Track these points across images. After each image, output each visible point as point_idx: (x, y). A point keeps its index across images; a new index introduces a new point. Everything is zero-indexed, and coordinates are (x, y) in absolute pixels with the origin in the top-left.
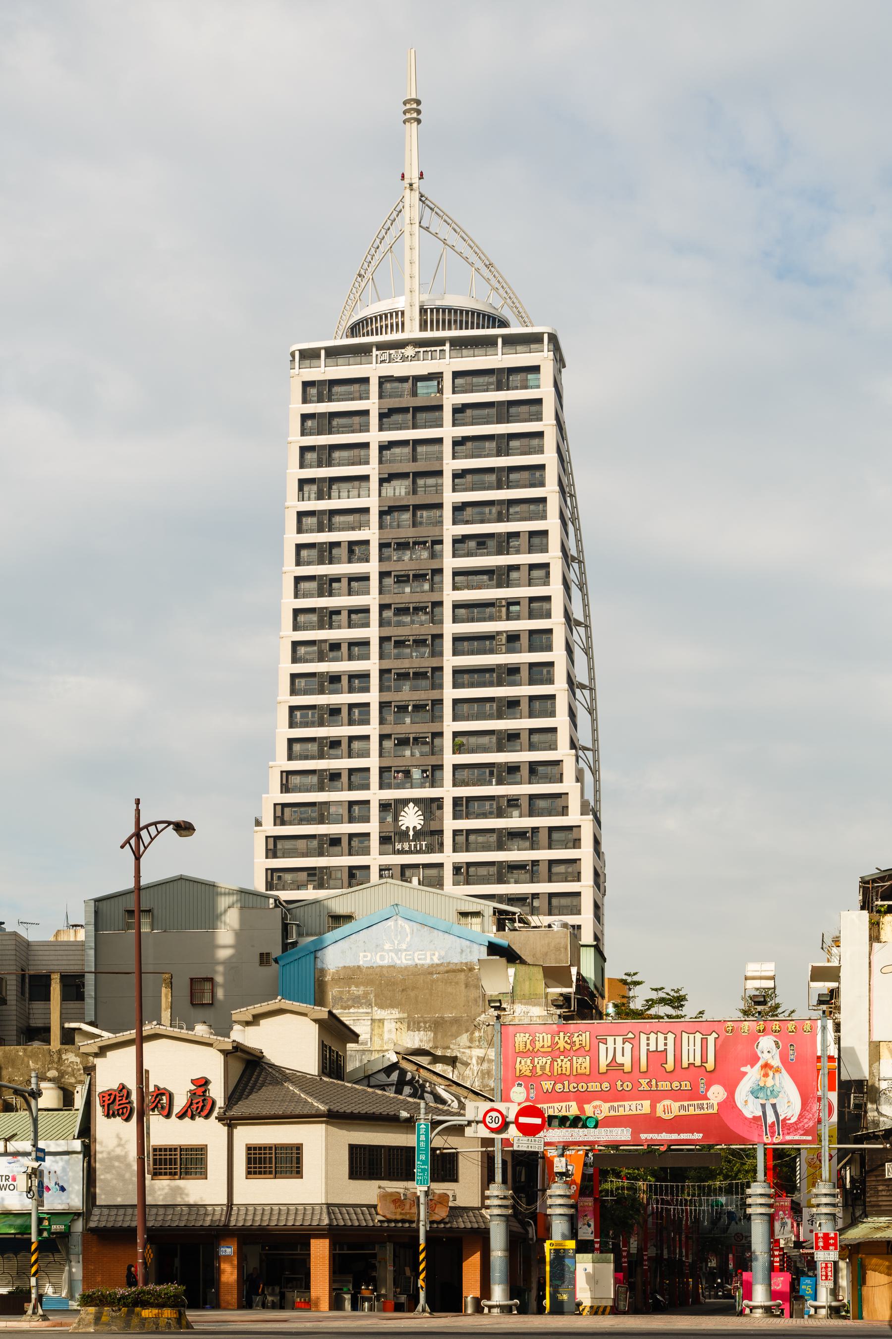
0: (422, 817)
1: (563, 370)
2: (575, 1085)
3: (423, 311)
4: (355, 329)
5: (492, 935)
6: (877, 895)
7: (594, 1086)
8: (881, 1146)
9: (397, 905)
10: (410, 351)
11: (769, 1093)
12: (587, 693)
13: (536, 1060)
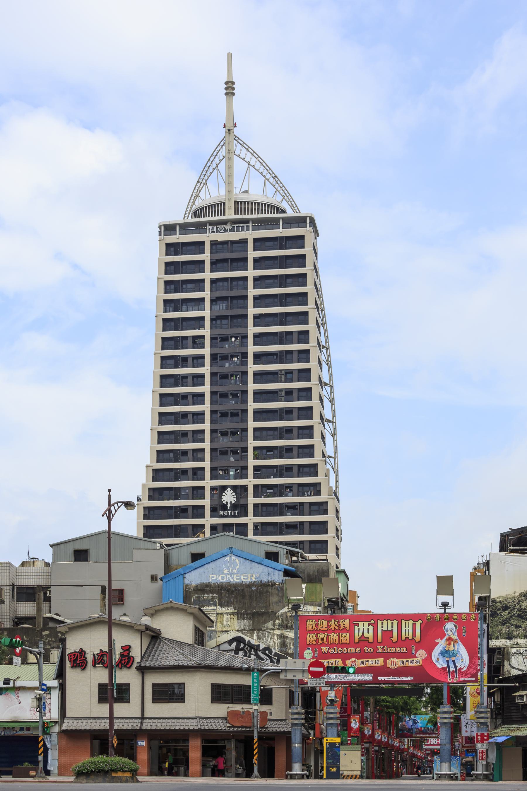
1: (317, 238)
2: (341, 649)
3: (236, 203)
4: (196, 214)
6: (510, 543)
7: (352, 650)
8: (513, 684)
9: (231, 548)
10: (229, 227)
11: (451, 654)
12: (331, 424)
13: (318, 635)
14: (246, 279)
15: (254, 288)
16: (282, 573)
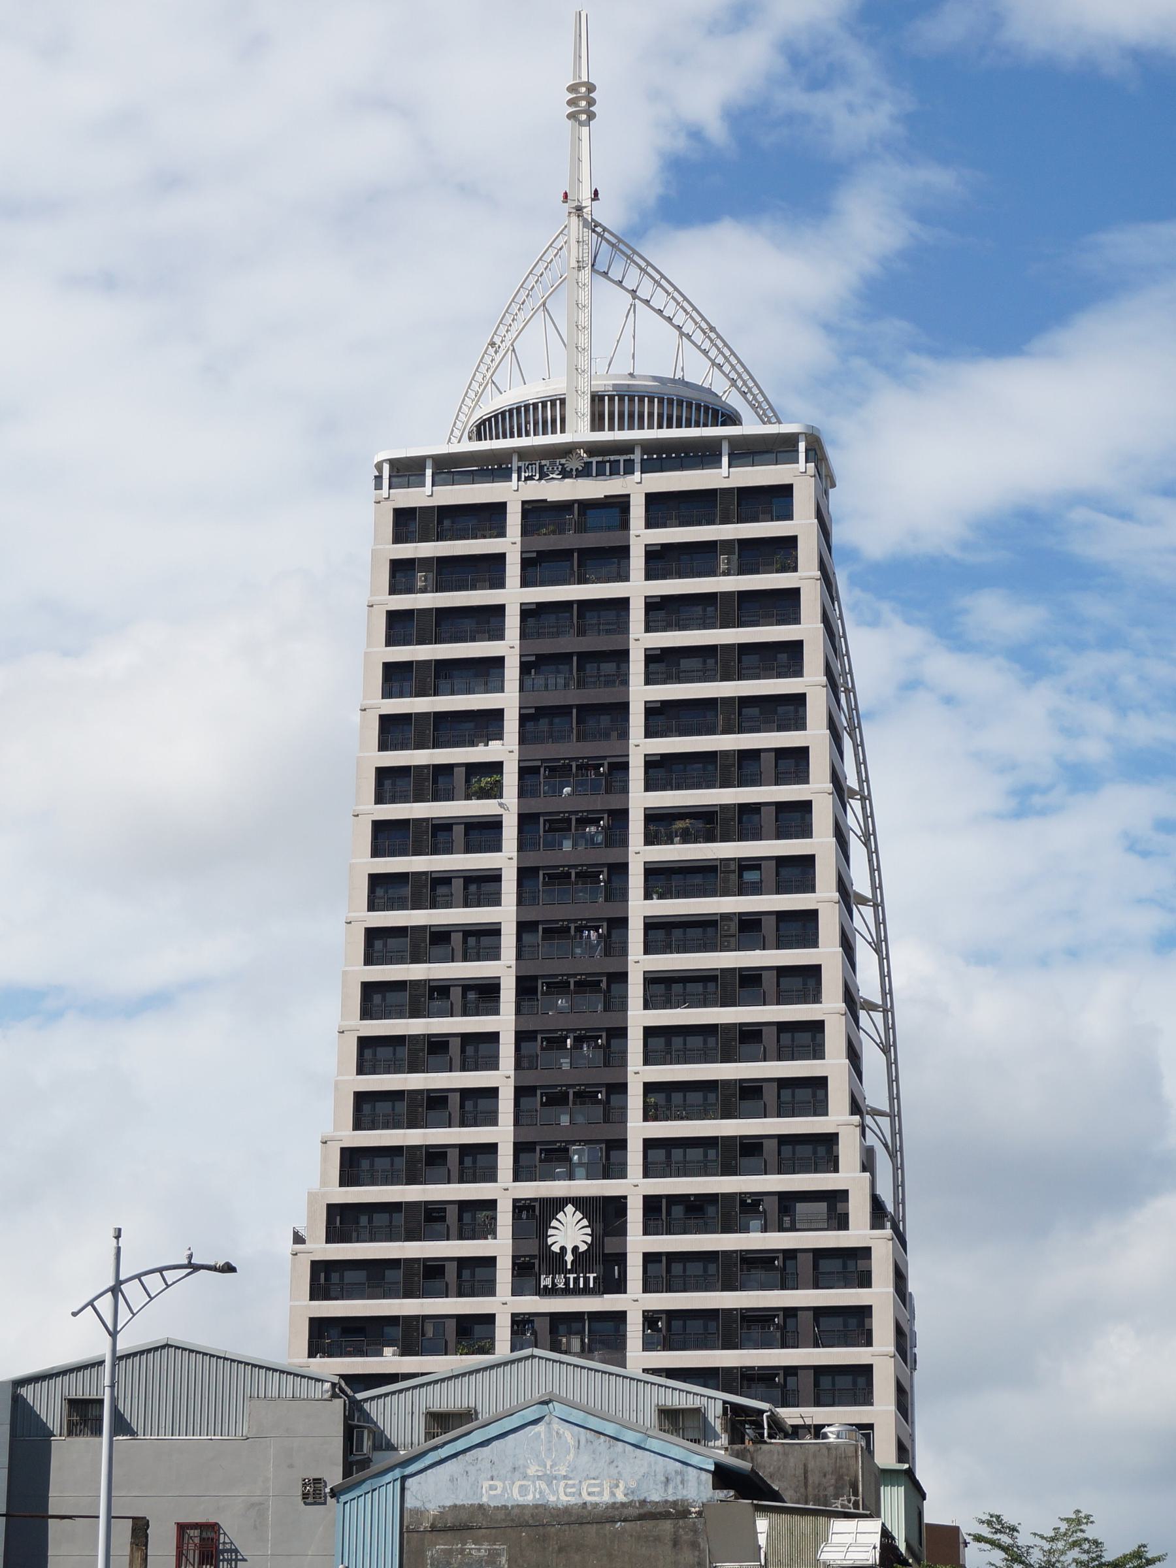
0: (589, 1231)
1: (831, 491)
4: (481, 430)
5: (719, 1451)
14: (622, 604)
15: (648, 629)
16: (708, 1478)
